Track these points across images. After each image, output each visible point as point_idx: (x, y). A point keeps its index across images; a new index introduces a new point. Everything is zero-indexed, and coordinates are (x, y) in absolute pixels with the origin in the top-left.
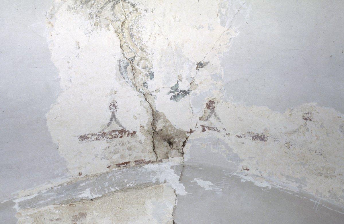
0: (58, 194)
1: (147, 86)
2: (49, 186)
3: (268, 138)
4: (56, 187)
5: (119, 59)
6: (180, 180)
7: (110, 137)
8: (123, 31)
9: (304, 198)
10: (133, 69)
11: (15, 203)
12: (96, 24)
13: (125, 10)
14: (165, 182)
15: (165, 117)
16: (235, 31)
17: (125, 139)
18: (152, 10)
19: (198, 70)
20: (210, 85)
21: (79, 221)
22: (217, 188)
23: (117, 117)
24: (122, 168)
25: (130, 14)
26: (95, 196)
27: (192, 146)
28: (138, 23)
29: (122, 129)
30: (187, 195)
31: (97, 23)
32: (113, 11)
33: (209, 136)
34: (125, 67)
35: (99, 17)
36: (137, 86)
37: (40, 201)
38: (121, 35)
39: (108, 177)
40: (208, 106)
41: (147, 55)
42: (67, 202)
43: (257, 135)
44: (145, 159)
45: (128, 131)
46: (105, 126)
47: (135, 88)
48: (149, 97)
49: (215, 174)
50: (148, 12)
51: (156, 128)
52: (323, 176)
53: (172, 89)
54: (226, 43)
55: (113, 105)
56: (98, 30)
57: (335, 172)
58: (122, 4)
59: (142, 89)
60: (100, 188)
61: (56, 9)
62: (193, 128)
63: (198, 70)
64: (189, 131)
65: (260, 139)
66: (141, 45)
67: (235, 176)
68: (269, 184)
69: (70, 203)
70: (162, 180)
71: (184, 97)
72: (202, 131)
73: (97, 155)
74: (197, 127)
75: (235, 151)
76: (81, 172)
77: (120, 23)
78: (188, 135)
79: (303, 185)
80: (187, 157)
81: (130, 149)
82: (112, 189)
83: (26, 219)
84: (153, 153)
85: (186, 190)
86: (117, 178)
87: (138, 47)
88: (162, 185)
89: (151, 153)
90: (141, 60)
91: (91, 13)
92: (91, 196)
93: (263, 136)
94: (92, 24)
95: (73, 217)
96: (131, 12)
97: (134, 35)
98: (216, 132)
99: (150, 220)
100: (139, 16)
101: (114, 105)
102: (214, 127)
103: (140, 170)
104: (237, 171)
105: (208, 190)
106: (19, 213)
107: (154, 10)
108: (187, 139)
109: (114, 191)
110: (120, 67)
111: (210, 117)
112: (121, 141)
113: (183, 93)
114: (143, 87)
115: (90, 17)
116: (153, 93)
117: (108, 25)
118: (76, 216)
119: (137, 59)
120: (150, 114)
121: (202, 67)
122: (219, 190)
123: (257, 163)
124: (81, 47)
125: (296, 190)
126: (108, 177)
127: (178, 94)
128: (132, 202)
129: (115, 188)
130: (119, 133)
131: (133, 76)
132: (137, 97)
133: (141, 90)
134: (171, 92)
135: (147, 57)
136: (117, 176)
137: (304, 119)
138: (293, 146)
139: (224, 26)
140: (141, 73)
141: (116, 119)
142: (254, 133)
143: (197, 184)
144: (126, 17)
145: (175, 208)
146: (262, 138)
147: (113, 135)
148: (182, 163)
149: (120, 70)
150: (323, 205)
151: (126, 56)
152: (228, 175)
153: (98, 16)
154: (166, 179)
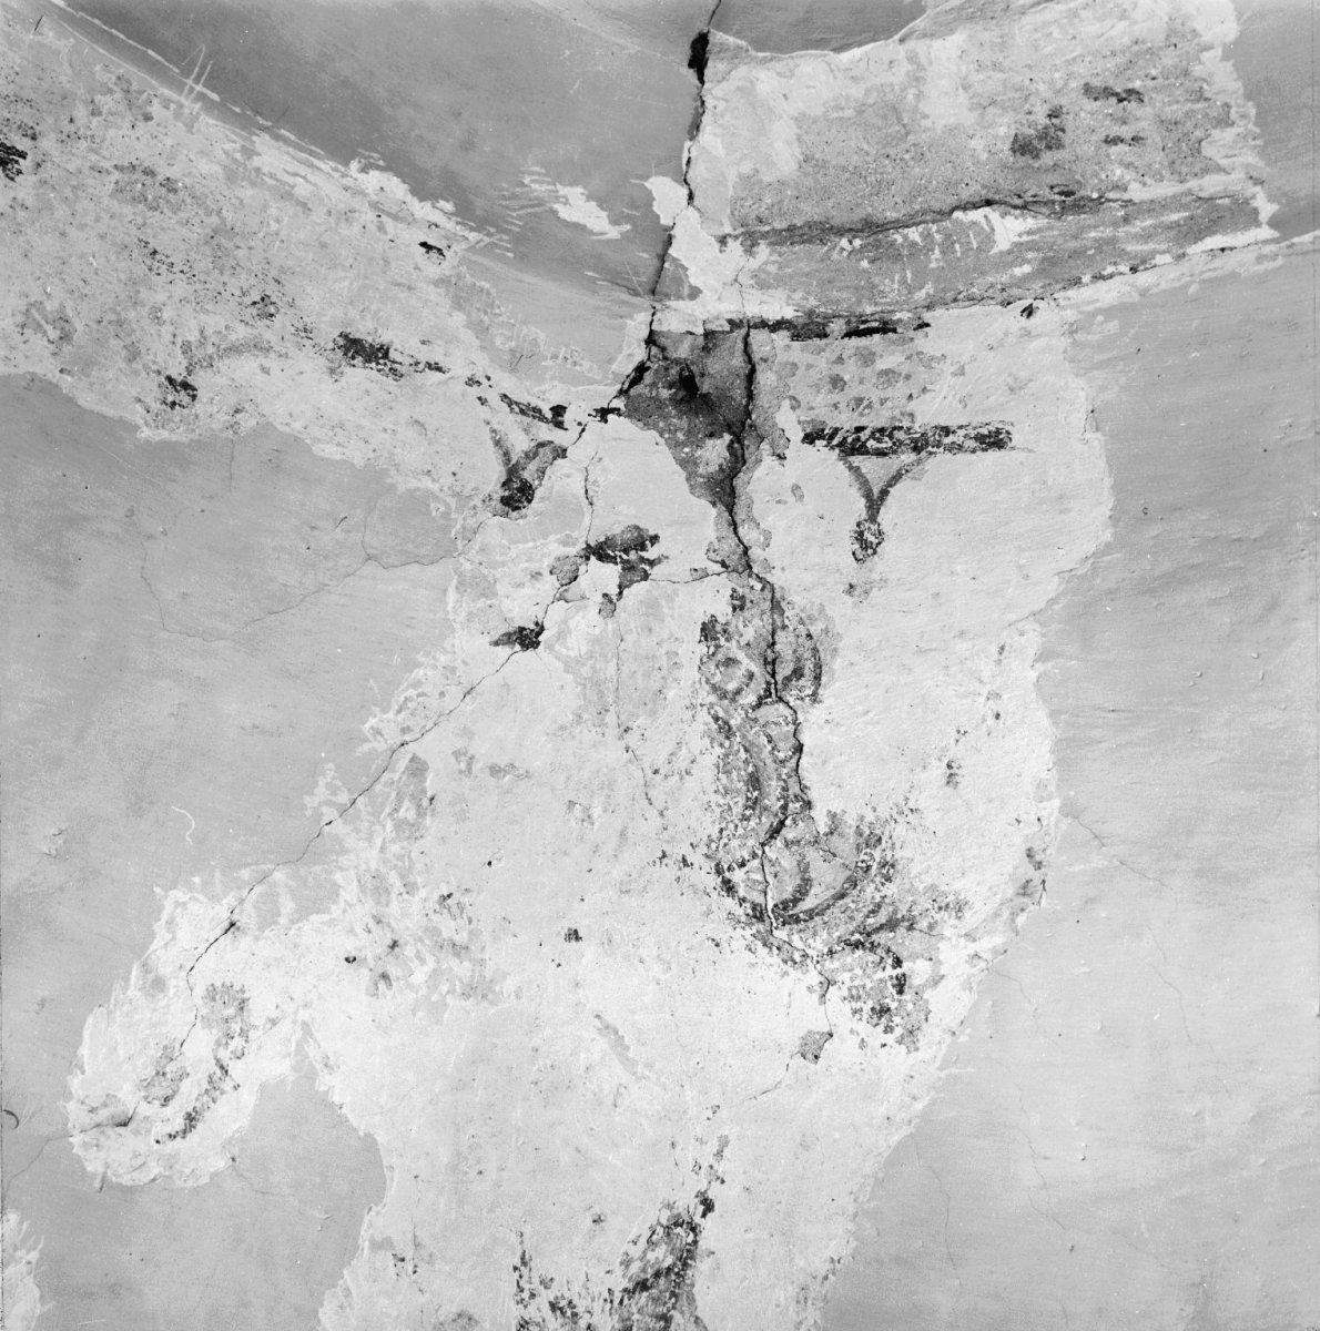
0: (1112, 241)
1: (732, 596)
2: (1143, 278)
3: (331, 345)
4: (1121, 274)
5: (816, 705)
6: (669, 241)
7: (899, 435)
8: (782, 802)
9: (237, 110)
10: (771, 664)
11: (1274, 223)
12: (872, 841)
13: (759, 877)
14: (723, 240)
15: (687, 480)
16: (380, 733)
17: (845, 421)
18: (665, 861)
19: (537, 624)
20: (504, 564)
21: (1040, 127)
22: (540, 189)
23: (863, 501)
24: (877, 317)
25: (744, 860)
26: (976, 215)
27: (610, 361)
28: (723, 825)
29: (851, 459)
30: (647, 178)
31: (867, 846)
32: (803, 879)
33: (543, 388)
34: (798, 673)
35: (859, 864)
36: (769, 603)
37: (1177, 224)
38: (790, 792)
39: (929, 288)
40: (526, 492)
41: (712, 705)
42: (1079, 206)
43: (370, 361)
44: (787, 341)
45: (832, 448)
46: (909, 474)
47: (778, 595)
48: (733, 561)
49: (536, 242)
50: (680, 858)
51: (730, 447)
52: (160, 178)
53: (645, 571)
54: (421, 699)
55: (866, 545)
56: (870, 817)
57: (117, 183)
58: (769, 897)
59: (752, 587)
60: (957, 246)
61: (1006, 914)
62: (594, 424)
63: (537, 624)
64: (611, 417)
65: (363, 347)
66: (727, 743)
67: (472, 229)
68: (356, 179)
69: (1070, 201)
70: (735, 247)
71: (607, 539)
72: (565, 408)
73: (954, 374)
74: (580, 424)
75: (459, 318)
76: (1024, 319)
77: (789, 833)
78: (619, 403)
79: (238, 156)
80: (638, 327)
81: (837, 382)
82: (914, 234)
83: (1231, 156)
84: (756, 357)
85: (649, 199)
86: (896, 278)
87: (738, 739)
88: (735, 230)
89: (766, 361)
90: (738, 692)
91: (883, 884)
92: (990, 217)
93: (350, 355)
94: (889, 845)
95: (1060, 146)
96: (742, 865)
97: (746, 783)
98: (514, 398)
99: (784, 95)
100: (713, 846)
101: (865, 545)
102: (520, 418)
103: (812, 302)
104: (464, 246)
105: (571, 185)
106: (1259, 182)
107: (658, 861)
108: (627, 392)
109: (907, 227)
110: (818, 678)
111: (527, 454)
112: (861, 415)
113: (610, 552)
114: (747, 596)
115: (891, 871)
116: (718, 568)
117: (832, 833)
118: (1049, 147)
119: (749, 698)
120: (743, 498)
121: (522, 629)
122: (533, 181)
123: (387, 262)
124: (944, 765)
125: (262, 141)
126: (929, 288)
127: (626, 551)
128: (847, 175)
129: (906, 237)
130: (864, 444)
131: (776, 638)
132: (776, 563)
133: (758, 586)
134: (652, 563)
135: (713, 698)
136: (896, 286)
137: (195, 389)
138: (248, 300)
139: (414, 759)
140: (748, 644)
141: (868, 495)
142: (379, 371)
143: (608, 216)
144: (764, 852)
145: (695, 128)
146: (353, 347)
147: (887, 439)
148: (658, 306)
149: (819, 666)
150: (177, 71)
151: (788, 712)
152: (498, 237)
153: (862, 868)
154: (721, 251)
